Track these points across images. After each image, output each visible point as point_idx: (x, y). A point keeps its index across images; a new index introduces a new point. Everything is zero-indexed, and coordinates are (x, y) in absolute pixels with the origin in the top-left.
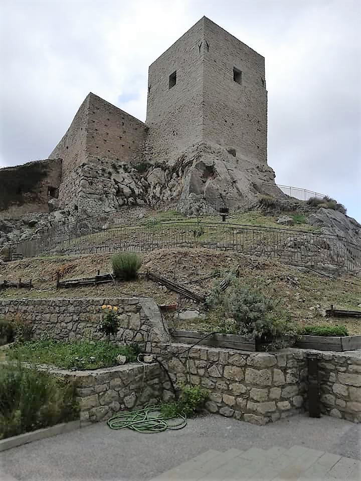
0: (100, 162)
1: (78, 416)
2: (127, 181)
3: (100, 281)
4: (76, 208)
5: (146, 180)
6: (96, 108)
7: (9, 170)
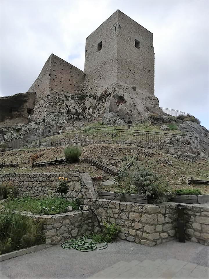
1: (45, 241)
2: (73, 105)
3: (57, 163)
4: (44, 121)
5: (84, 104)
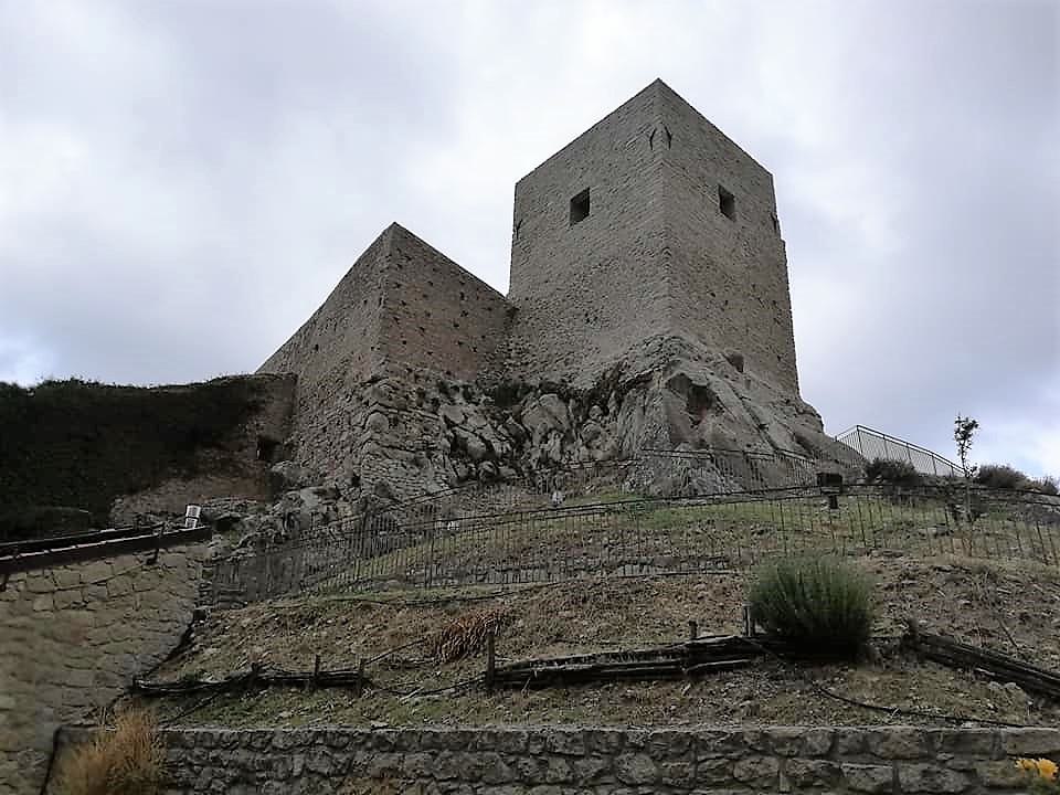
0: (412, 375)
2: (477, 427)
3: (697, 663)
4: (356, 481)
5: (519, 420)
6: (400, 261)
7: (172, 391)
